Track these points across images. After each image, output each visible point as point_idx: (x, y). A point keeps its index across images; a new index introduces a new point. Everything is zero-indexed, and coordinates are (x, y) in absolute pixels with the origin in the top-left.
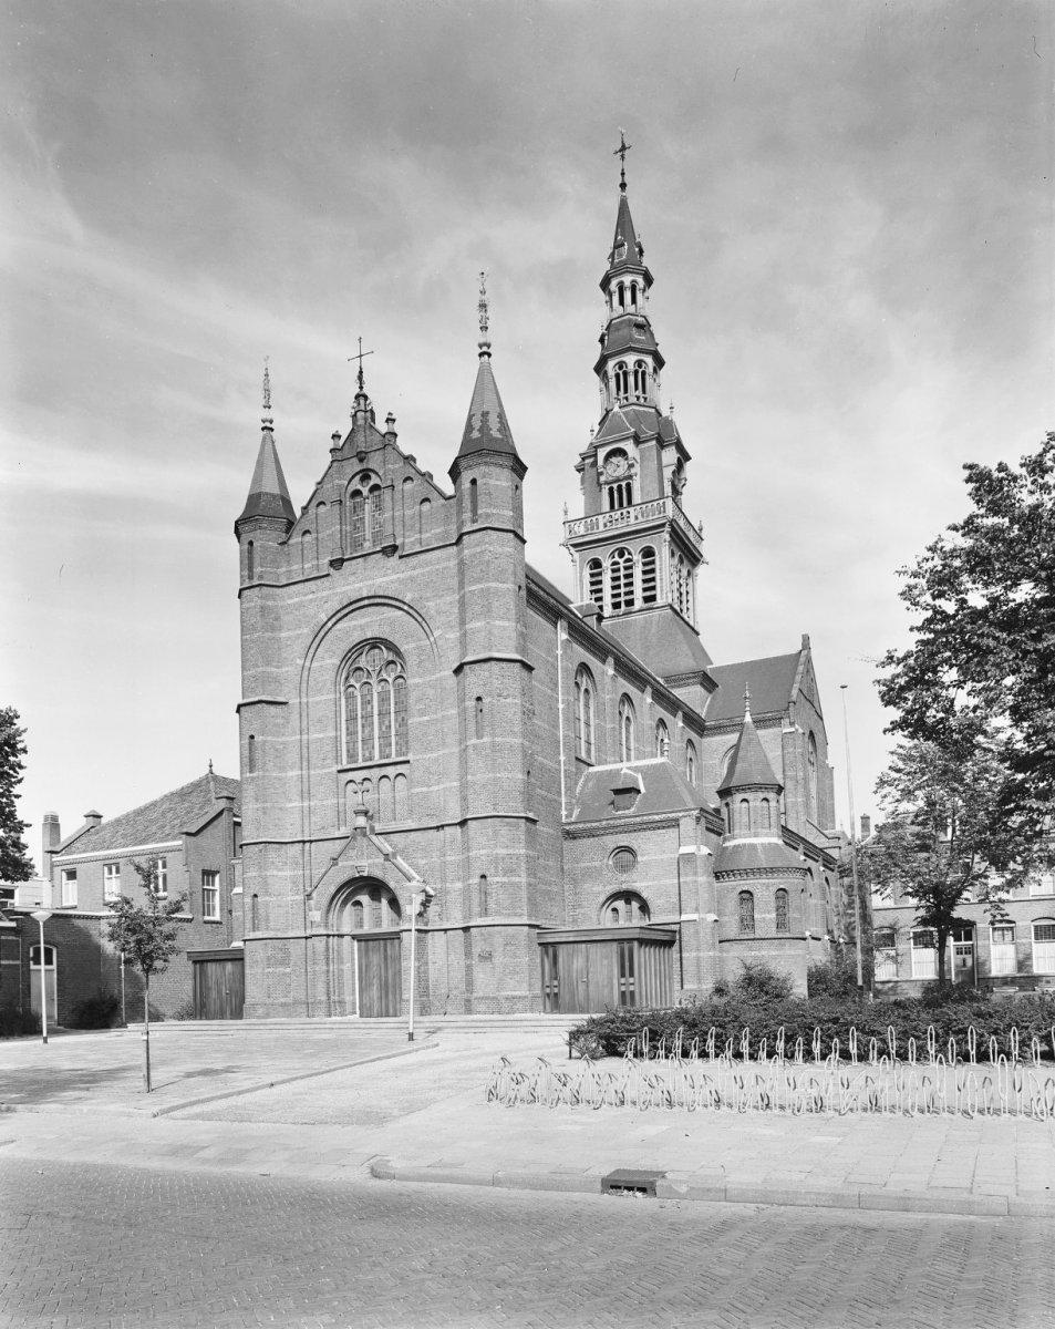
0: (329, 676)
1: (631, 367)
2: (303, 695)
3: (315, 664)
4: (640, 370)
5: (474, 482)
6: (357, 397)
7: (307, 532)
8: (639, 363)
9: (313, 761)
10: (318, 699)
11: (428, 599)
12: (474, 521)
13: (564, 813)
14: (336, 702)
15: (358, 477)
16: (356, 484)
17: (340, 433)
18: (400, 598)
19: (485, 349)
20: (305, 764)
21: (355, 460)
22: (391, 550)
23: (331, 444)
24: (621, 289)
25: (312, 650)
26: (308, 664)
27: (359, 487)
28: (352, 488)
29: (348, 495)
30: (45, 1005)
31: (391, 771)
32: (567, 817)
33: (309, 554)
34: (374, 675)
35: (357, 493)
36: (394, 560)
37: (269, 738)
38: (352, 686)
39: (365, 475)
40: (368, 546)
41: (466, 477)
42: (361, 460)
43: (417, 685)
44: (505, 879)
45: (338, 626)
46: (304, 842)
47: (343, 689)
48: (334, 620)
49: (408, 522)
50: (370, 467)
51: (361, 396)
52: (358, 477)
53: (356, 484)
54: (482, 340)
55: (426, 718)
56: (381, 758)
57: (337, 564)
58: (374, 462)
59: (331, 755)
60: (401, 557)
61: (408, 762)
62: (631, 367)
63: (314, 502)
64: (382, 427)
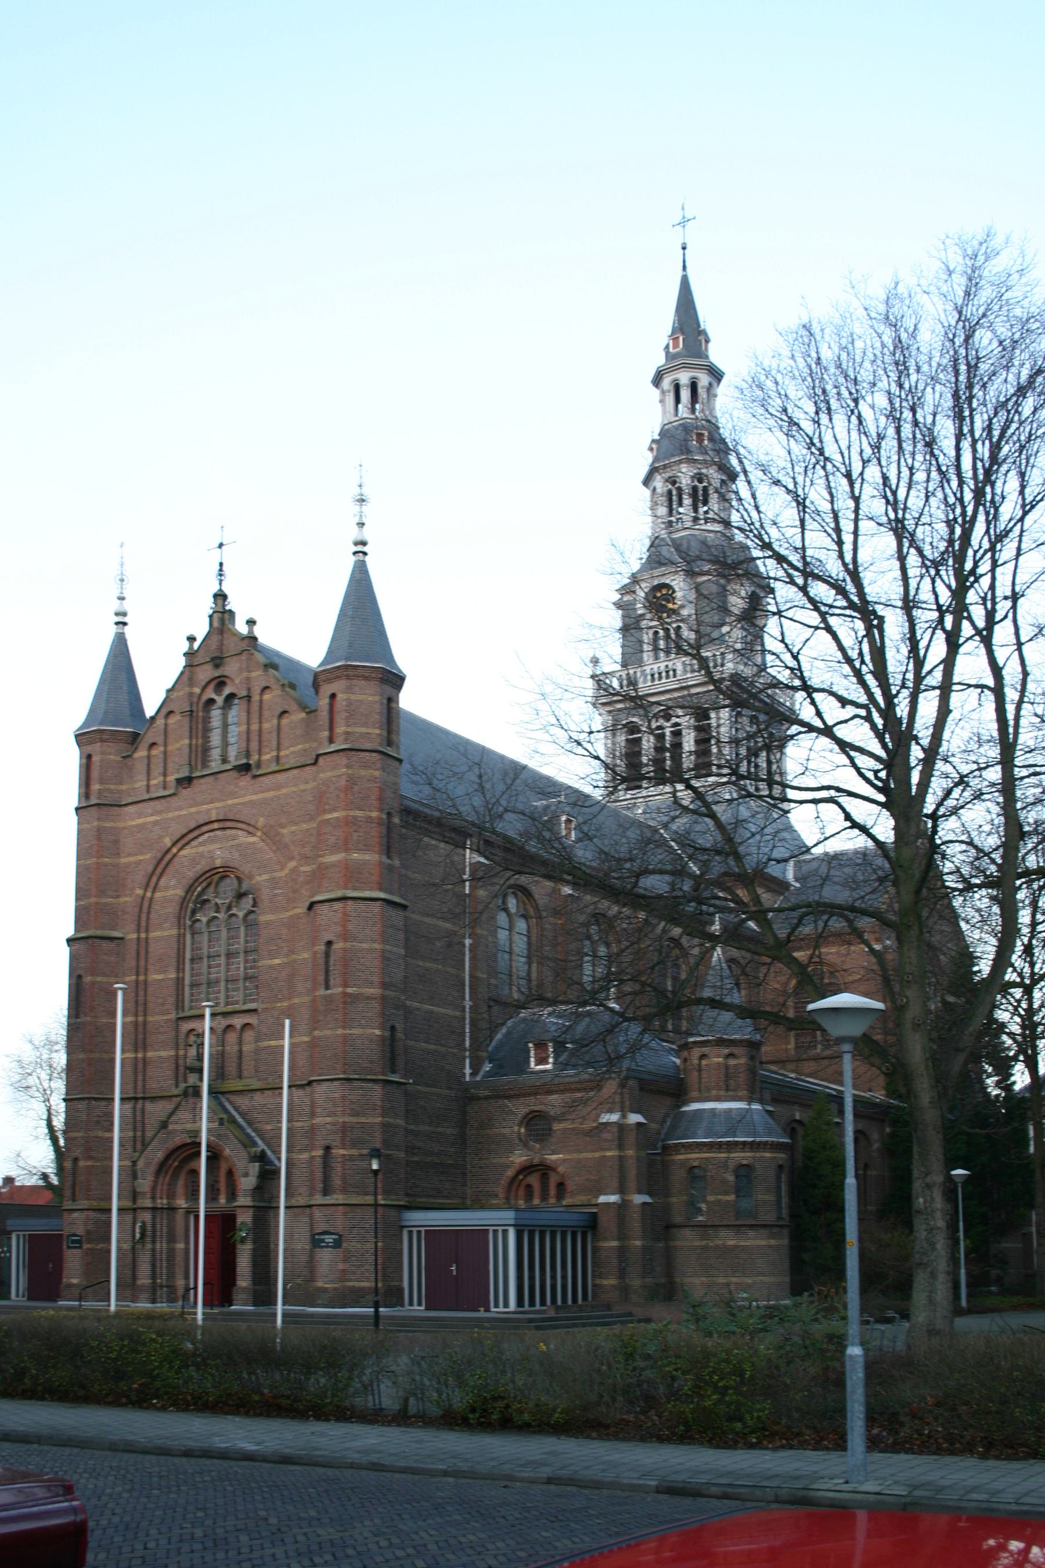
0: (172, 909)
1: (685, 481)
2: (143, 929)
3: (158, 895)
4: (700, 486)
5: (333, 696)
6: (216, 596)
7: (153, 744)
8: (699, 478)
9: (150, 1005)
10: (158, 934)
11: (283, 826)
12: (331, 740)
13: (468, 1071)
14: (180, 938)
15: (212, 686)
16: (210, 694)
17: (196, 635)
18: (252, 822)
19: (360, 548)
20: (141, 1008)
21: (209, 667)
22: (245, 768)
23: (185, 646)
24: (677, 388)
25: (154, 879)
26: (149, 894)
27: (213, 696)
28: (205, 698)
29: (201, 705)
30: (862, 1516)
31: (238, 1021)
32: (471, 1074)
33: (157, 769)
34: (223, 909)
35: (211, 702)
36: (245, 781)
37: (99, 979)
38: (199, 920)
39: (220, 683)
40: (215, 765)
41: (327, 690)
42: (217, 666)
43: (268, 923)
44: (354, 1152)
45: (183, 852)
46: (136, 1099)
47: (188, 923)
48: (179, 845)
49: (265, 736)
50: (226, 674)
51: (220, 597)
52: (212, 686)
53: (210, 694)
54: (359, 538)
55: (277, 961)
56: (227, 1004)
57: (186, 781)
58: (231, 668)
59: (171, 1000)
60: (255, 777)
61: (255, 1010)
62: (685, 481)
63: (164, 711)
64: (242, 628)
